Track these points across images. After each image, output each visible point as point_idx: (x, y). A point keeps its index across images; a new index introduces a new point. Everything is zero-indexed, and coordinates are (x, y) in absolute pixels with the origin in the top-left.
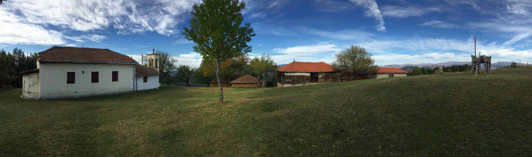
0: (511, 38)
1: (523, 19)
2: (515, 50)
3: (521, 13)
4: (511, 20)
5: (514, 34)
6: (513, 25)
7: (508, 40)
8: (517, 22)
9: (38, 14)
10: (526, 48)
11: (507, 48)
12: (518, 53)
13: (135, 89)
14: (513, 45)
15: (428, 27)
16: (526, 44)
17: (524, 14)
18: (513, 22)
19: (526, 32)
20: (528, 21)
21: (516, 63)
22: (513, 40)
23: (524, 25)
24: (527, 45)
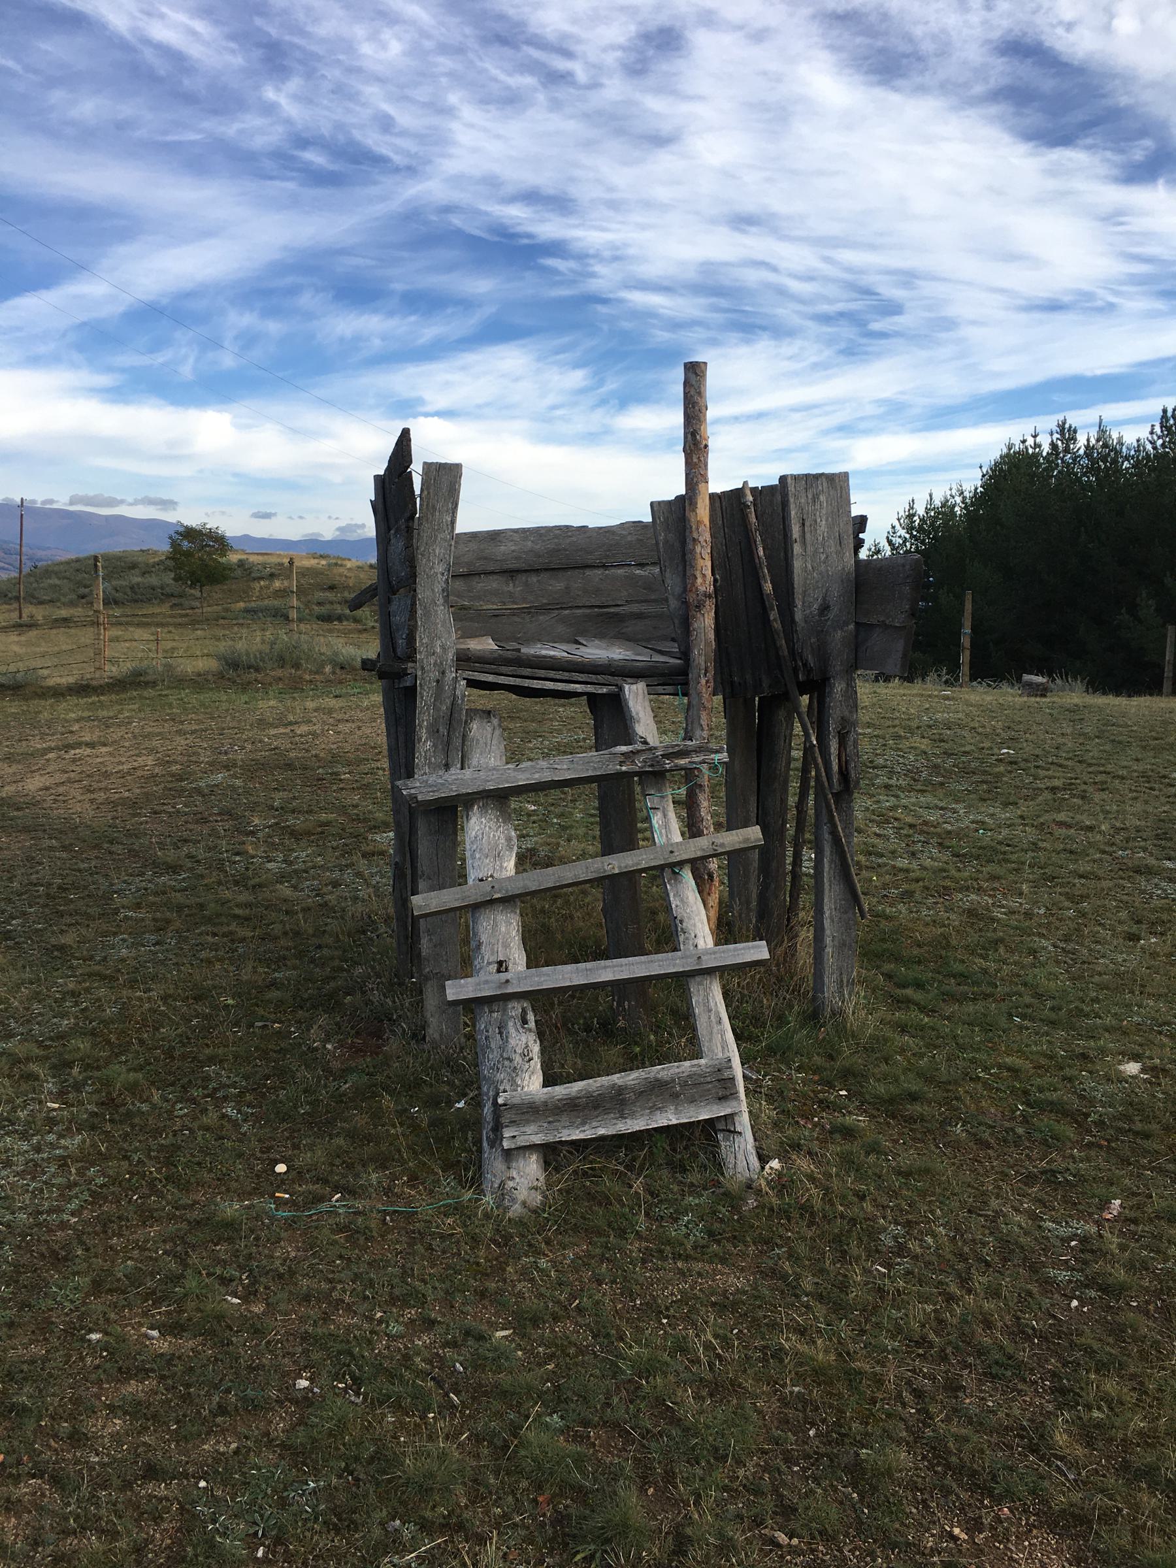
0: (80, 268)
1: (190, 99)
2: (117, 394)
3: (161, 33)
4: (67, 78)
5: (97, 228)
6: (86, 138)
7: (43, 278)
8: (126, 110)
9: (175, 601)
10: (214, 389)
11: (34, 361)
12: (149, 421)
13: (640, 836)
14: (94, 341)
15: (1030, 684)
16: (215, 343)
17: (195, 51)
18: (89, 108)
19: (207, 233)
20: (230, 129)
21: (219, 542)
22: (95, 292)
23: (198, 161)
24: (228, 360)
